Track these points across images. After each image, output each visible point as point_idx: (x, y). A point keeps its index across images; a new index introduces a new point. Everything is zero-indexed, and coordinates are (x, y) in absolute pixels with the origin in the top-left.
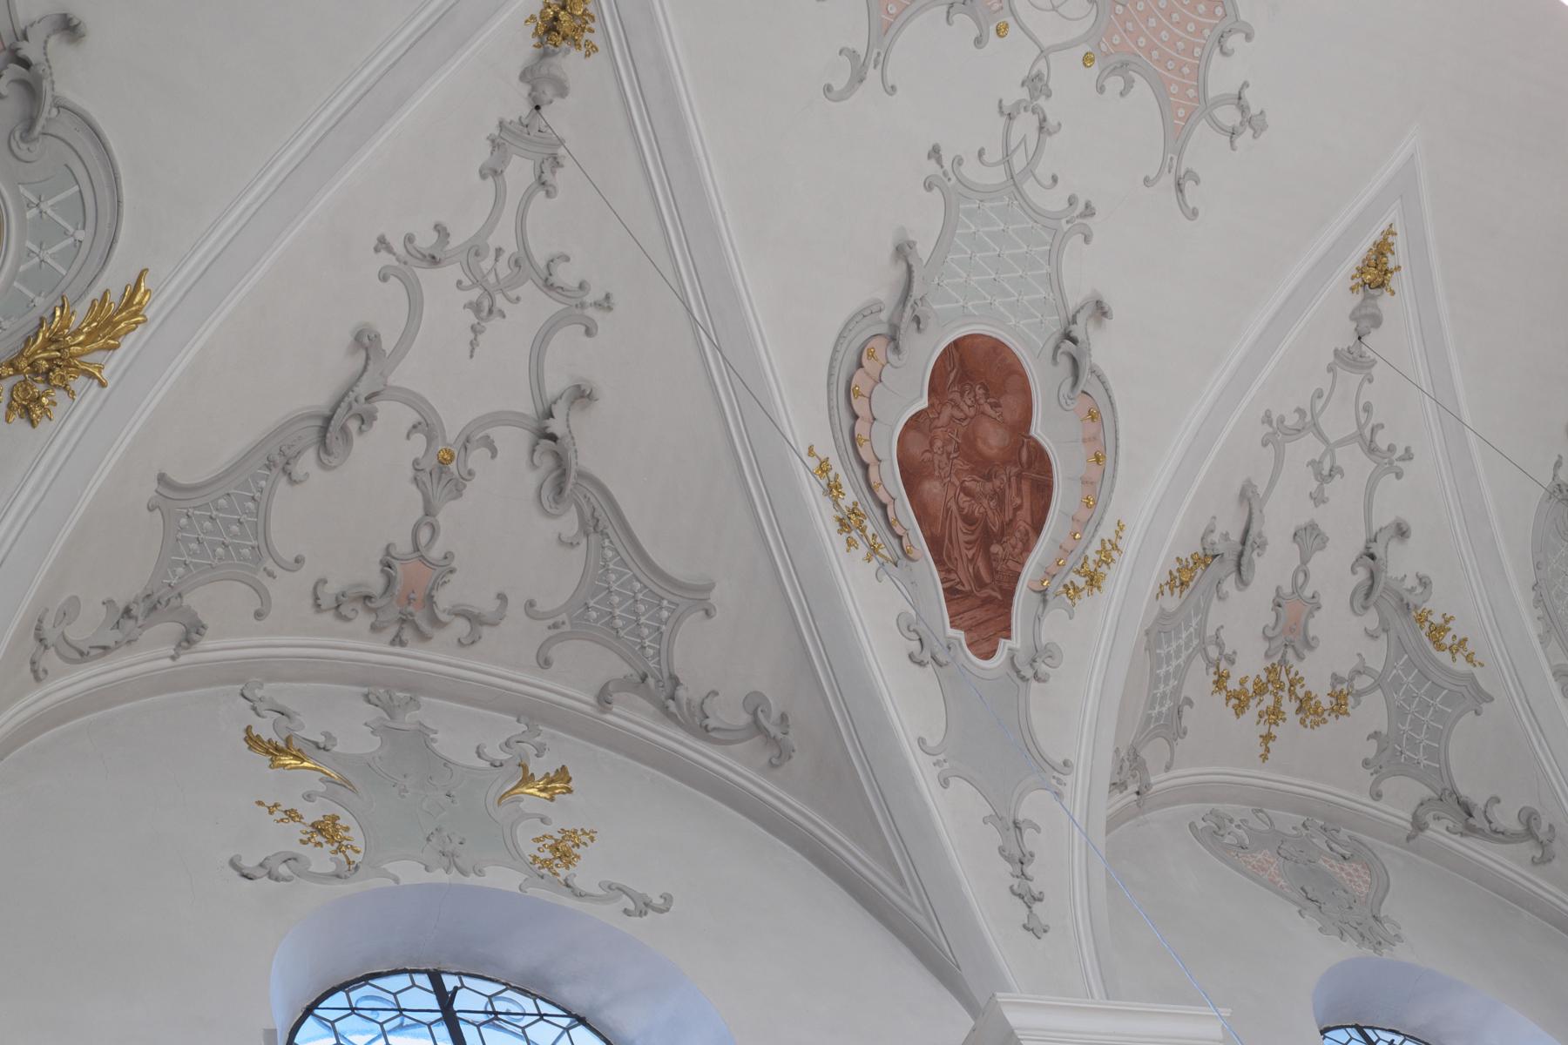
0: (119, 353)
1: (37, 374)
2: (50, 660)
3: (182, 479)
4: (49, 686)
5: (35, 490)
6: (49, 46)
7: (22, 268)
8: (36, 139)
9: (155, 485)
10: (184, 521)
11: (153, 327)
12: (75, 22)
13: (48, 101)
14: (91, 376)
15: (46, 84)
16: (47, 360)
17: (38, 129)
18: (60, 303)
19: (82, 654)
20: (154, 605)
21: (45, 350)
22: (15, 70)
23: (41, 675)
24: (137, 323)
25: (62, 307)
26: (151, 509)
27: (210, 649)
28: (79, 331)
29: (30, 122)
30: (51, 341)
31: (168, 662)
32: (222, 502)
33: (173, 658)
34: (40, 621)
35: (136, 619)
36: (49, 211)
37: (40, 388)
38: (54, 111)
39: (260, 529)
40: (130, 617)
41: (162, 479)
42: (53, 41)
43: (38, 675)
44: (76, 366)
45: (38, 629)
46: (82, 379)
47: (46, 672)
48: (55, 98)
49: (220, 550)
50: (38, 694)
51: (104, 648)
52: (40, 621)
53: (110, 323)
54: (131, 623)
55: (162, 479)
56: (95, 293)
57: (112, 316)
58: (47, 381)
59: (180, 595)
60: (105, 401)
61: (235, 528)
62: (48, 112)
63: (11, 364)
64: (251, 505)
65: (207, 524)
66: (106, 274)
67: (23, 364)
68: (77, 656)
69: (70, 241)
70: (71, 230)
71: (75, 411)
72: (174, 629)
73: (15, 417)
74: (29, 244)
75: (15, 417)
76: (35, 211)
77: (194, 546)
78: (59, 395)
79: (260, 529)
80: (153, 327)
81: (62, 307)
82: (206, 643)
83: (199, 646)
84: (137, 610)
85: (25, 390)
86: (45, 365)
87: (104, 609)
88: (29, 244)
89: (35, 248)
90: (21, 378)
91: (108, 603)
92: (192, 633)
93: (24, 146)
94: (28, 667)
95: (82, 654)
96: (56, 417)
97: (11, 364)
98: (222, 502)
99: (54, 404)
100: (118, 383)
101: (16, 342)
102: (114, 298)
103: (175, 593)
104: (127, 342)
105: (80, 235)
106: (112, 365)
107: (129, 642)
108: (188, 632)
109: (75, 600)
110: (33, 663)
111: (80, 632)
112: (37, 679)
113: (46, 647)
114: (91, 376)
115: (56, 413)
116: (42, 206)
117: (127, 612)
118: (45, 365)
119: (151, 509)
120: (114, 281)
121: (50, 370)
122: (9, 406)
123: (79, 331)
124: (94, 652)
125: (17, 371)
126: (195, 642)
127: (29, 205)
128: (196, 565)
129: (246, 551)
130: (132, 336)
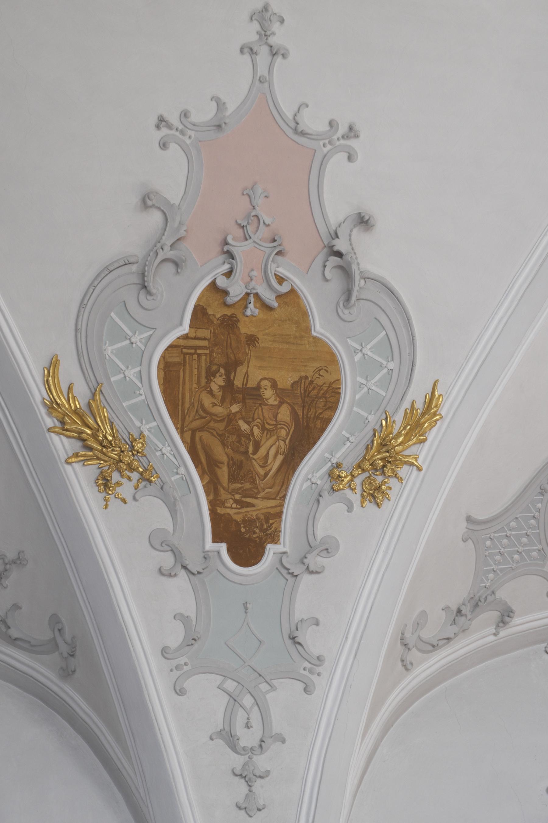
0: (427, 443)
1: (376, 470)
2: (414, 655)
3: (481, 517)
4: (416, 671)
5: (386, 552)
6: (353, 237)
7: (357, 397)
8: (354, 305)
9: (465, 524)
10: (488, 543)
11: (448, 420)
12: (367, 218)
13: (357, 277)
14: (412, 464)
15: (354, 267)
16: (381, 459)
17: (354, 298)
18: (384, 417)
19: (433, 646)
20: (476, 604)
21: (379, 452)
22: (334, 260)
23: (409, 666)
24: (436, 421)
25: (386, 419)
26: (465, 541)
27: (520, 624)
28: (399, 434)
29: (348, 293)
30: (382, 445)
31: (492, 638)
32: (513, 524)
33: (495, 635)
34: (403, 634)
35: (466, 616)
36: (369, 353)
37: (379, 479)
38: (362, 282)
39: (542, 536)
40: (462, 615)
41: (469, 519)
42: (355, 231)
43: (407, 667)
44: (400, 460)
45: (402, 639)
46: (406, 468)
47: (412, 664)
48: (361, 272)
49: (516, 557)
50: (410, 677)
51: (448, 639)
52: (403, 634)
53: (420, 421)
54: (463, 618)
55: (469, 519)
56: (406, 405)
57: (420, 419)
58: (383, 473)
59: (493, 593)
60: (422, 481)
61: (524, 540)
62: (358, 283)
63: (359, 466)
64: (533, 522)
65: (505, 541)
66: (411, 389)
67: (367, 465)
68: (431, 648)
69: (385, 371)
70: (385, 363)
71: (405, 489)
72: (495, 615)
73: (367, 503)
74: (359, 379)
75: (367, 503)
76: (360, 355)
77: (498, 557)
78: (393, 482)
79: (542, 536)
80: (448, 420)
81: (386, 419)
82: (516, 620)
83: (512, 624)
84: (464, 610)
85: (370, 483)
86: (380, 463)
87: (444, 612)
88: (359, 379)
89: (364, 381)
90: (366, 474)
91: (446, 609)
92: (506, 616)
93: (346, 311)
94: (400, 664)
95: (433, 646)
96: (392, 498)
97: (359, 466)
98: (513, 524)
99: (390, 488)
100: (429, 466)
101: (360, 450)
102: (420, 406)
103: (489, 592)
104: (432, 435)
105: (391, 365)
106: (424, 453)
107: (464, 631)
108: (503, 616)
109: (424, 614)
110: (403, 661)
111: (429, 633)
112: (407, 669)
113: (409, 649)
114: (412, 464)
115: (392, 494)
116: (364, 351)
117: (459, 611)
118: (380, 463)
119: (465, 541)
120: (417, 394)
121: (384, 466)
122: (362, 496)
123: (399, 434)
124: (441, 643)
125: (364, 471)
126: (508, 623)
127: (356, 352)
128: (501, 570)
129: (534, 554)
130: (435, 430)
